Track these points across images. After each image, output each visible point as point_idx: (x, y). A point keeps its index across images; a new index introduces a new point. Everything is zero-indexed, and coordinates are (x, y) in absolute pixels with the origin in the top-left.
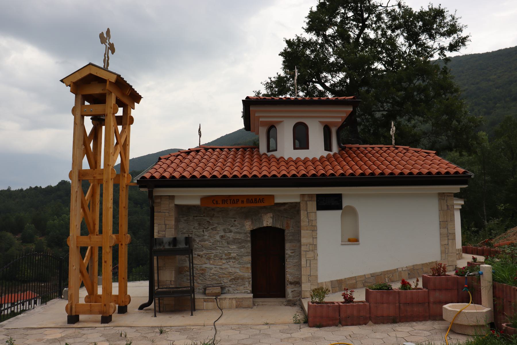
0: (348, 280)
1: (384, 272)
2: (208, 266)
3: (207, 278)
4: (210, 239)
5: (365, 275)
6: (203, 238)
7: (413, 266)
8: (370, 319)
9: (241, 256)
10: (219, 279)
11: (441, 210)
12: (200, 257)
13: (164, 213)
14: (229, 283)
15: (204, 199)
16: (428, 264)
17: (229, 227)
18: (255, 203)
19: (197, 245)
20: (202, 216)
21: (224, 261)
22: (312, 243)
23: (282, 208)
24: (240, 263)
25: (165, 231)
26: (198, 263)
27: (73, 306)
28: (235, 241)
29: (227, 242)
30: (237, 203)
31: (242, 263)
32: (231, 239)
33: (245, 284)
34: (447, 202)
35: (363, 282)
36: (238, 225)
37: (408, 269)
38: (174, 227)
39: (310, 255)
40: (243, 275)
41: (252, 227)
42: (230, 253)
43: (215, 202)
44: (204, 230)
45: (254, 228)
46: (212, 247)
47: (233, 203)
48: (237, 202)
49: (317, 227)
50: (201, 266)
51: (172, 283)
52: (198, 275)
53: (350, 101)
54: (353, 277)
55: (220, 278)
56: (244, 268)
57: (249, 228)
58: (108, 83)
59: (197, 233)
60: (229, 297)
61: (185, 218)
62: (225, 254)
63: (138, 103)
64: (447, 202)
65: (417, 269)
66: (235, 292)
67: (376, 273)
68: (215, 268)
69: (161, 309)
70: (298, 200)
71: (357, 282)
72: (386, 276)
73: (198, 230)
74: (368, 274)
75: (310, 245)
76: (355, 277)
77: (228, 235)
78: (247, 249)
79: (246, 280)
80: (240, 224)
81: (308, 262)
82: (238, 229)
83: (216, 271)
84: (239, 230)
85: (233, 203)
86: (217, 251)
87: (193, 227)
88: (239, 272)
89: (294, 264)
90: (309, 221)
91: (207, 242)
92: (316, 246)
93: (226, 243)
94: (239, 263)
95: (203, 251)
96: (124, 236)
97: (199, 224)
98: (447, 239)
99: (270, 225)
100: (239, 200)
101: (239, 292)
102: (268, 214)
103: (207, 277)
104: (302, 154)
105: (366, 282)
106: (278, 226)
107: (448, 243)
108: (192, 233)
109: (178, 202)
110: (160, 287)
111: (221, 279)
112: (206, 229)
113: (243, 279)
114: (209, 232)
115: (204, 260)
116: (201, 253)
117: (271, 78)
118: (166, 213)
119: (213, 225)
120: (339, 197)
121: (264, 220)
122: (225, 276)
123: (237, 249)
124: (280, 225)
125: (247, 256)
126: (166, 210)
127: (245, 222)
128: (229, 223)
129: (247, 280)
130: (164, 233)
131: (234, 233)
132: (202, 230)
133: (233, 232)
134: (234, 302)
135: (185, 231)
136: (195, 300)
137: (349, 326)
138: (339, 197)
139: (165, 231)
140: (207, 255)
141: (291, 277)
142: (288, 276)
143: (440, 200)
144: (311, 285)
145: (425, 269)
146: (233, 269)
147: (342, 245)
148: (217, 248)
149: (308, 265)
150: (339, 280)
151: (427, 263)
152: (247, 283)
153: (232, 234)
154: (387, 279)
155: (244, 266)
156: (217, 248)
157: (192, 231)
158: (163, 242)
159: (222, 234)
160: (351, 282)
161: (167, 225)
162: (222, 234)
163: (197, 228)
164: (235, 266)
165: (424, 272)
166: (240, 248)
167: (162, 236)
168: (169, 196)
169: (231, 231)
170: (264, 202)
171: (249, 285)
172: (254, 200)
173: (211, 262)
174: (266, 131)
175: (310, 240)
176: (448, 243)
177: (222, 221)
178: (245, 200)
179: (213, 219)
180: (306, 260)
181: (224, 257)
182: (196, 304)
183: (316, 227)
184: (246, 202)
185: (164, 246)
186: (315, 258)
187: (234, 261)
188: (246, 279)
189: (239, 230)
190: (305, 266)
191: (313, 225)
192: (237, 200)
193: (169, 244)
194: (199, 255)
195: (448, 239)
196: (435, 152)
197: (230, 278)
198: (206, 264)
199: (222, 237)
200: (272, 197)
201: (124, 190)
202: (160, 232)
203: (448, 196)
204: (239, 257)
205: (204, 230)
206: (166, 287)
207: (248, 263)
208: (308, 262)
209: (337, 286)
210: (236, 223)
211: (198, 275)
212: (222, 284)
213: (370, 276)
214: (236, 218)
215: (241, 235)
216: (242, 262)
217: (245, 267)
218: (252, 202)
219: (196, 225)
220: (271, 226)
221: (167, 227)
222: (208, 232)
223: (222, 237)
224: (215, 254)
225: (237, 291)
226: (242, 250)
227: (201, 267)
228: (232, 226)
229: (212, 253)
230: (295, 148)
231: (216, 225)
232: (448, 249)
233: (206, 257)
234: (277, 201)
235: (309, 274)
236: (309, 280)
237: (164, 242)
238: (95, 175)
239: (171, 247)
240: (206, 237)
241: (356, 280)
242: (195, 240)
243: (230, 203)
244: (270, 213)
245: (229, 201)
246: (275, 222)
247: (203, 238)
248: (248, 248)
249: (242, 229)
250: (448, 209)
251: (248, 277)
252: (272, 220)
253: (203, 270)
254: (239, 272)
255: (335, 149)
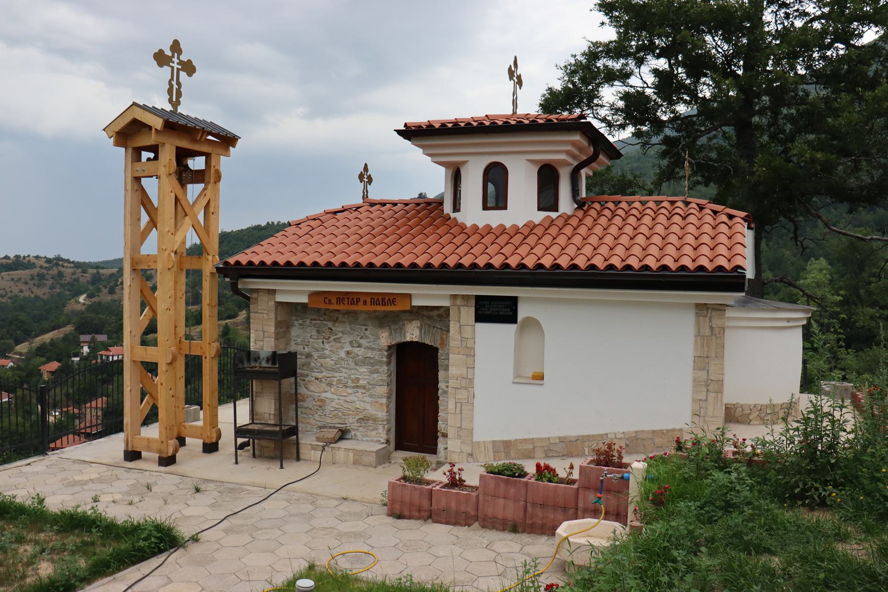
0: (521, 443)
1: (582, 436)
2: (328, 395)
3: (327, 413)
4: (332, 356)
5: (549, 438)
6: (322, 353)
7: (636, 432)
8: (476, 518)
9: (374, 385)
10: (343, 417)
11: (698, 335)
12: (318, 382)
13: (261, 315)
14: (356, 425)
15: (313, 295)
16: (664, 431)
17: (358, 339)
18: (382, 305)
19: (315, 364)
20: (321, 319)
21: (350, 391)
22: (465, 376)
23: (435, 313)
24: (372, 395)
25: (263, 341)
26: (315, 390)
27: (129, 439)
28: (366, 361)
29: (355, 362)
30: (357, 304)
32: (360, 357)
34: (710, 321)
35: (546, 449)
36: (370, 336)
37: (626, 436)
38: (273, 336)
39: (462, 395)
42: (358, 379)
43: (327, 301)
44: (325, 341)
45: (393, 343)
46: (334, 367)
47: (351, 304)
48: (357, 302)
49: (474, 351)
50: (319, 394)
51: (272, 417)
52: (316, 407)
53: (570, 123)
54: (530, 439)
55: (344, 415)
58: (153, 131)
59: (315, 344)
60: (344, 447)
61: (300, 321)
62: (352, 380)
63: (234, 147)
64: (710, 321)
65: (643, 439)
66: (364, 439)
67: (568, 437)
68: (339, 399)
69: (256, 452)
70: (446, 303)
71: (536, 449)
72: (586, 444)
73: (317, 341)
74: (555, 438)
75: (462, 378)
76: (533, 439)
77: (356, 350)
80: (373, 335)
81: (459, 405)
82: (370, 342)
83: (338, 404)
85: (351, 304)
86: (341, 374)
87: (309, 335)
88: (370, 408)
90: (463, 339)
91: (328, 360)
92: (471, 381)
93: (353, 364)
94: (371, 396)
95: (322, 372)
96: (208, 345)
97: (318, 332)
98: (706, 390)
99: (416, 340)
100: (359, 299)
101: (369, 439)
102: (414, 322)
103: (328, 412)
104: (495, 218)
105: (549, 450)
106: (428, 342)
107: (707, 398)
108: (307, 344)
109: (280, 298)
110: (255, 421)
111: (346, 417)
112: (327, 339)
113: (375, 420)
114: (331, 344)
115: (323, 386)
116: (320, 375)
117: (575, 56)
118: (265, 315)
119: (337, 335)
120: (513, 302)
122: (351, 413)
123: (368, 374)
125: (381, 385)
126: (265, 310)
127: (380, 332)
128: (358, 333)
129: (381, 423)
130: (262, 343)
131: (365, 348)
132: (322, 341)
133: (364, 346)
134: (351, 455)
135: (299, 340)
136: (300, 445)
137: (443, 524)
138: (514, 301)
139: (263, 341)
140: (328, 379)
143: (697, 315)
144: (461, 443)
145: (658, 441)
146: (362, 404)
147: (514, 383)
148: (341, 369)
149: (458, 411)
150: (506, 441)
151: (663, 430)
152: (381, 427)
153: (362, 349)
154: (586, 449)
156: (341, 369)
157: (309, 342)
158: (259, 358)
159: (349, 348)
160: (525, 447)
161: (266, 333)
162: (349, 348)
163: (315, 337)
164: (365, 399)
165: (655, 446)
166: (372, 372)
167: (259, 348)
168: (269, 290)
169: (360, 346)
170: (395, 305)
172: (380, 300)
173: (333, 390)
174: (452, 175)
175: (463, 371)
176: (707, 398)
177: (349, 329)
178: (369, 300)
179: (337, 324)
180: (456, 403)
181: (350, 384)
182: (302, 451)
183: (472, 351)
184: (370, 304)
185: (260, 363)
186: (470, 401)
187: (363, 391)
188: (379, 421)
190: (454, 412)
191: (468, 346)
192: (357, 299)
193: (268, 360)
194: (317, 379)
195: (707, 391)
196: (744, 214)
197: (357, 417)
198: (326, 392)
199: (348, 353)
200: (409, 296)
201: (208, 279)
202: (257, 342)
203: (713, 309)
204: (370, 386)
205: (325, 341)
206: (264, 422)
208: (459, 405)
209: (503, 450)
210: (368, 333)
211: (316, 407)
212: (346, 424)
213: (558, 441)
214: (368, 326)
215: (375, 352)
218: (378, 303)
219: (314, 333)
220: (417, 342)
221: (265, 335)
222: (329, 344)
223: (348, 353)
224: (338, 378)
225: (367, 438)
226: (375, 375)
227: (319, 396)
228: (362, 338)
229: (334, 377)
230: (485, 207)
231: (340, 335)
232: (707, 408)
233: (327, 382)
234: (415, 303)
235: (460, 426)
236: (458, 435)
237: (261, 357)
238: (149, 263)
239: (270, 366)
240: (327, 352)
241: (534, 444)
242: (312, 355)
243: (348, 304)
244: (415, 319)
245: (346, 300)
247: (322, 353)
250: (712, 334)
253: (321, 401)
254: (370, 408)
255: (566, 205)
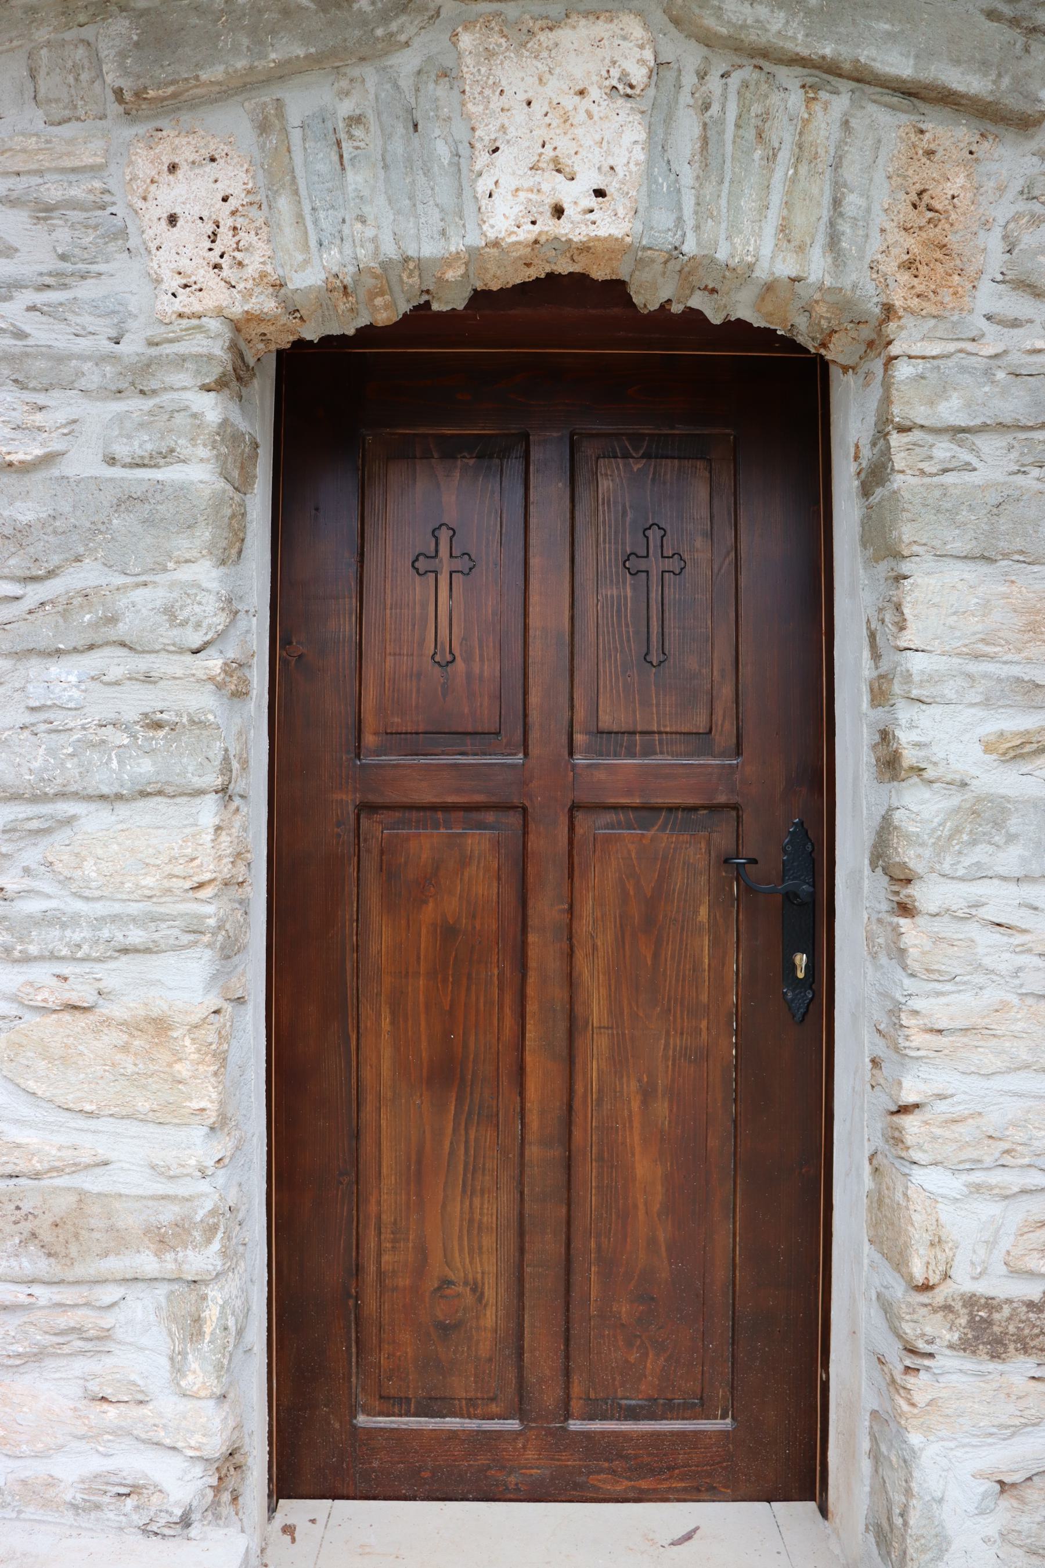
31: (54, 938)
33: (105, 1336)
40: (78, 1168)
41: (254, 264)
56: (82, 1021)
57: (205, 276)
78: (158, 664)
79: (114, 1265)
84: (29, 323)
89: (927, 1362)
121: (485, 133)
124: (784, 229)
127: (144, 164)
129: (147, 1262)
141: (988, 1209)
142: (933, 1198)
155: (81, 993)
171: (177, 1365)
189: (29, 323)
207: (166, 932)
216: (48, 920)
217: (116, 1010)
246: (688, 175)
248: (170, 635)
249: (85, 291)
251: (169, 1214)
252: (636, 132)
